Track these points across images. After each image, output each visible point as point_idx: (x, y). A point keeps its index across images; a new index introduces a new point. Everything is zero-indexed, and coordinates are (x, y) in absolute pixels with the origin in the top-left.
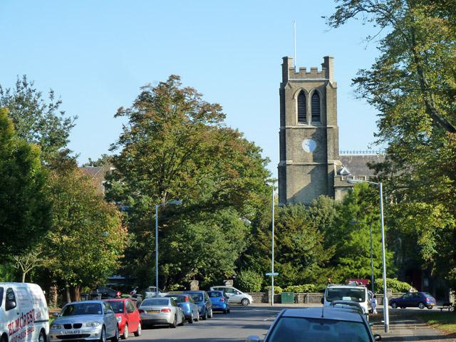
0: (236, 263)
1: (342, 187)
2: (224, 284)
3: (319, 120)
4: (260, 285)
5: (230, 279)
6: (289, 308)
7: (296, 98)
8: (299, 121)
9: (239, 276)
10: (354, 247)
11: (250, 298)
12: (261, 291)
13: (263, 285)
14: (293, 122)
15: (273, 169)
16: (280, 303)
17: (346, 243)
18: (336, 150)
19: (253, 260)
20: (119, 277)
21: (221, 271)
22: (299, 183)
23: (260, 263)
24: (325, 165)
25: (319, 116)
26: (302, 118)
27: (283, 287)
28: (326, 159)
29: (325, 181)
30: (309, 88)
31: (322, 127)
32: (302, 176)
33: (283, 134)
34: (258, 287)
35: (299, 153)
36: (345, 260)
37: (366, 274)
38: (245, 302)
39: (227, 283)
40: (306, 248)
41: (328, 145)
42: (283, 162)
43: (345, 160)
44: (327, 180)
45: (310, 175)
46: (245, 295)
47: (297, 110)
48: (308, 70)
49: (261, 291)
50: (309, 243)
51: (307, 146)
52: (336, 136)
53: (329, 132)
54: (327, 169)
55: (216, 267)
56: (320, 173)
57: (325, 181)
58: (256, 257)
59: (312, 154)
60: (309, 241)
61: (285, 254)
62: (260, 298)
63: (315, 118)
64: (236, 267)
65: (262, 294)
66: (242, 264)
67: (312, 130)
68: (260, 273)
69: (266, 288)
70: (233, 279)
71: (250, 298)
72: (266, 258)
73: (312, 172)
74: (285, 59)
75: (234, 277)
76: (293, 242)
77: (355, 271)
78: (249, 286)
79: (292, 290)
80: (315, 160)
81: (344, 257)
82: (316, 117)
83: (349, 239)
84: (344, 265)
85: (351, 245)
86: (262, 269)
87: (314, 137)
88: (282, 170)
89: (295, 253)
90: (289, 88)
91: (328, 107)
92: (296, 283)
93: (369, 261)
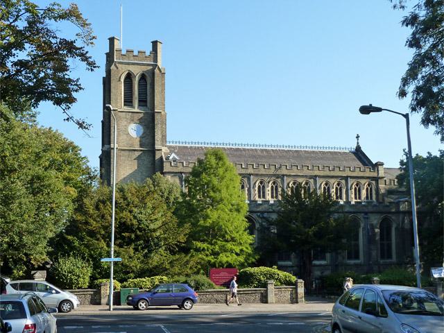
0: (51, 242)
1: (173, 173)
2: (32, 278)
3: (146, 106)
4: (87, 279)
5: (40, 268)
6: (105, 310)
7: (122, 80)
8: (125, 105)
9: (56, 264)
10: (212, 227)
11: (75, 300)
12: (89, 287)
13: (93, 278)
14: (118, 103)
15: (94, 164)
16: (120, 305)
17: (201, 222)
18: (164, 137)
19: (76, 244)
20: (121, 326)
21: (26, 254)
22: (124, 169)
23: (87, 246)
24: (153, 151)
25: (146, 101)
26: (128, 102)
27: (121, 281)
28: (154, 144)
29: (151, 162)
30: (137, 71)
31: (150, 111)
32: (127, 162)
33: (107, 113)
34: (85, 281)
35: (125, 137)
36: (199, 245)
37: (227, 262)
38: (66, 307)
39: (36, 275)
40: (152, 226)
41: (156, 130)
42: (107, 146)
43: (172, 149)
44: (154, 165)
45: (136, 161)
46: (66, 295)
47: (123, 93)
48: (136, 53)
49: (89, 287)
50: (156, 219)
51: (134, 131)
52: (164, 123)
53: (157, 117)
54: (154, 156)
55: (17, 249)
56: (147, 160)
57: (151, 162)
58: (81, 239)
59: (138, 139)
60: (156, 219)
61: (130, 234)
62: (89, 298)
63: (142, 104)
64: (50, 249)
65: (91, 291)
66: (60, 246)
67: (138, 114)
68: (88, 261)
69: (97, 282)
70: (47, 269)
71: (75, 300)
72: (98, 240)
73: (138, 158)
74: (112, 40)
75: (48, 266)
76: (135, 217)
77: (211, 259)
78: (71, 279)
79: (135, 286)
80: (141, 145)
81: (198, 240)
82: (143, 102)
83: (206, 217)
84: (198, 250)
85: (208, 225)
86: (91, 256)
87: (141, 121)
88: (106, 158)
89: (138, 233)
90: (115, 68)
91: (156, 91)
92: (141, 274)
93: (229, 246)
